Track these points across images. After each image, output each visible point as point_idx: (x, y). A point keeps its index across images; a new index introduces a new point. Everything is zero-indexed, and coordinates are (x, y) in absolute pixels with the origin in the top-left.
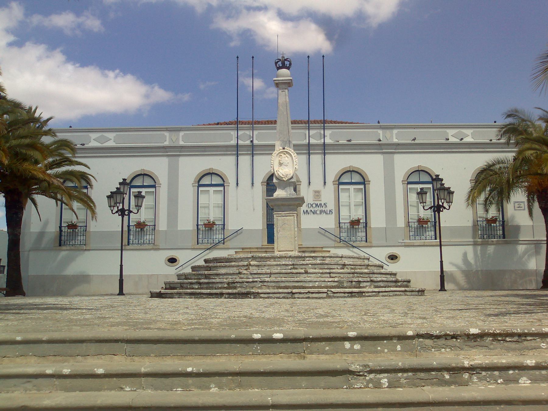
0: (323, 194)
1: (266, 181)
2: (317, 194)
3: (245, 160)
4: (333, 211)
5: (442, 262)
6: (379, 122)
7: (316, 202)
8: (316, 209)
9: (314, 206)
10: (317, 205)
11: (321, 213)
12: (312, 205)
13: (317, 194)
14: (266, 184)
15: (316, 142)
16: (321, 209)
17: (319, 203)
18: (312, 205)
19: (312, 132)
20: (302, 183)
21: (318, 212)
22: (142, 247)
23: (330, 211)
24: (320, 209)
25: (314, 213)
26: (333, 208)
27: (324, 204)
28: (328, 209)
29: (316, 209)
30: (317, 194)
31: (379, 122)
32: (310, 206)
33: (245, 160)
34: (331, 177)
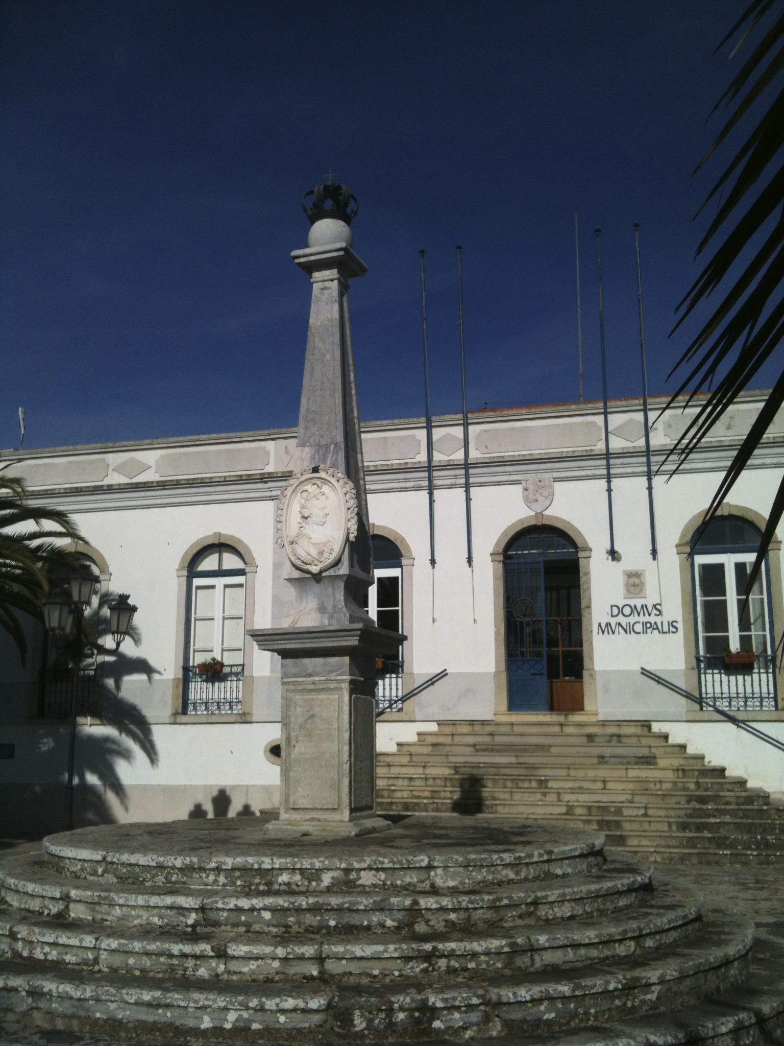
0: (650, 581)
1: (501, 550)
2: (633, 580)
3: (450, 500)
4: (680, 626)
5: (672, 332)
6: (486, 447)
7: (632, 602)
8: (632, 620)
9: (627, 611)
10: (634, 609)
11: (645, 631)
12: (621, 611)
13: (634, 582)
14: (501, 558)
15: (630, 445)
16: (647, 618)
17: (638, 603)
18: (621, 611)
19: (615, 420)
20: (593, 554)
21: (638, 628)
22: (215, 713)
23: (672, 624)
24: (642, 619)
25: (629, 629)
26: (680, 619)
27: (654, 606)
28: (667, 617)
29: (632, 620)
30: (634, 582)
31: (486, 447)
32: (615, 611)
33: (450, 500)
34: (672, 533)
